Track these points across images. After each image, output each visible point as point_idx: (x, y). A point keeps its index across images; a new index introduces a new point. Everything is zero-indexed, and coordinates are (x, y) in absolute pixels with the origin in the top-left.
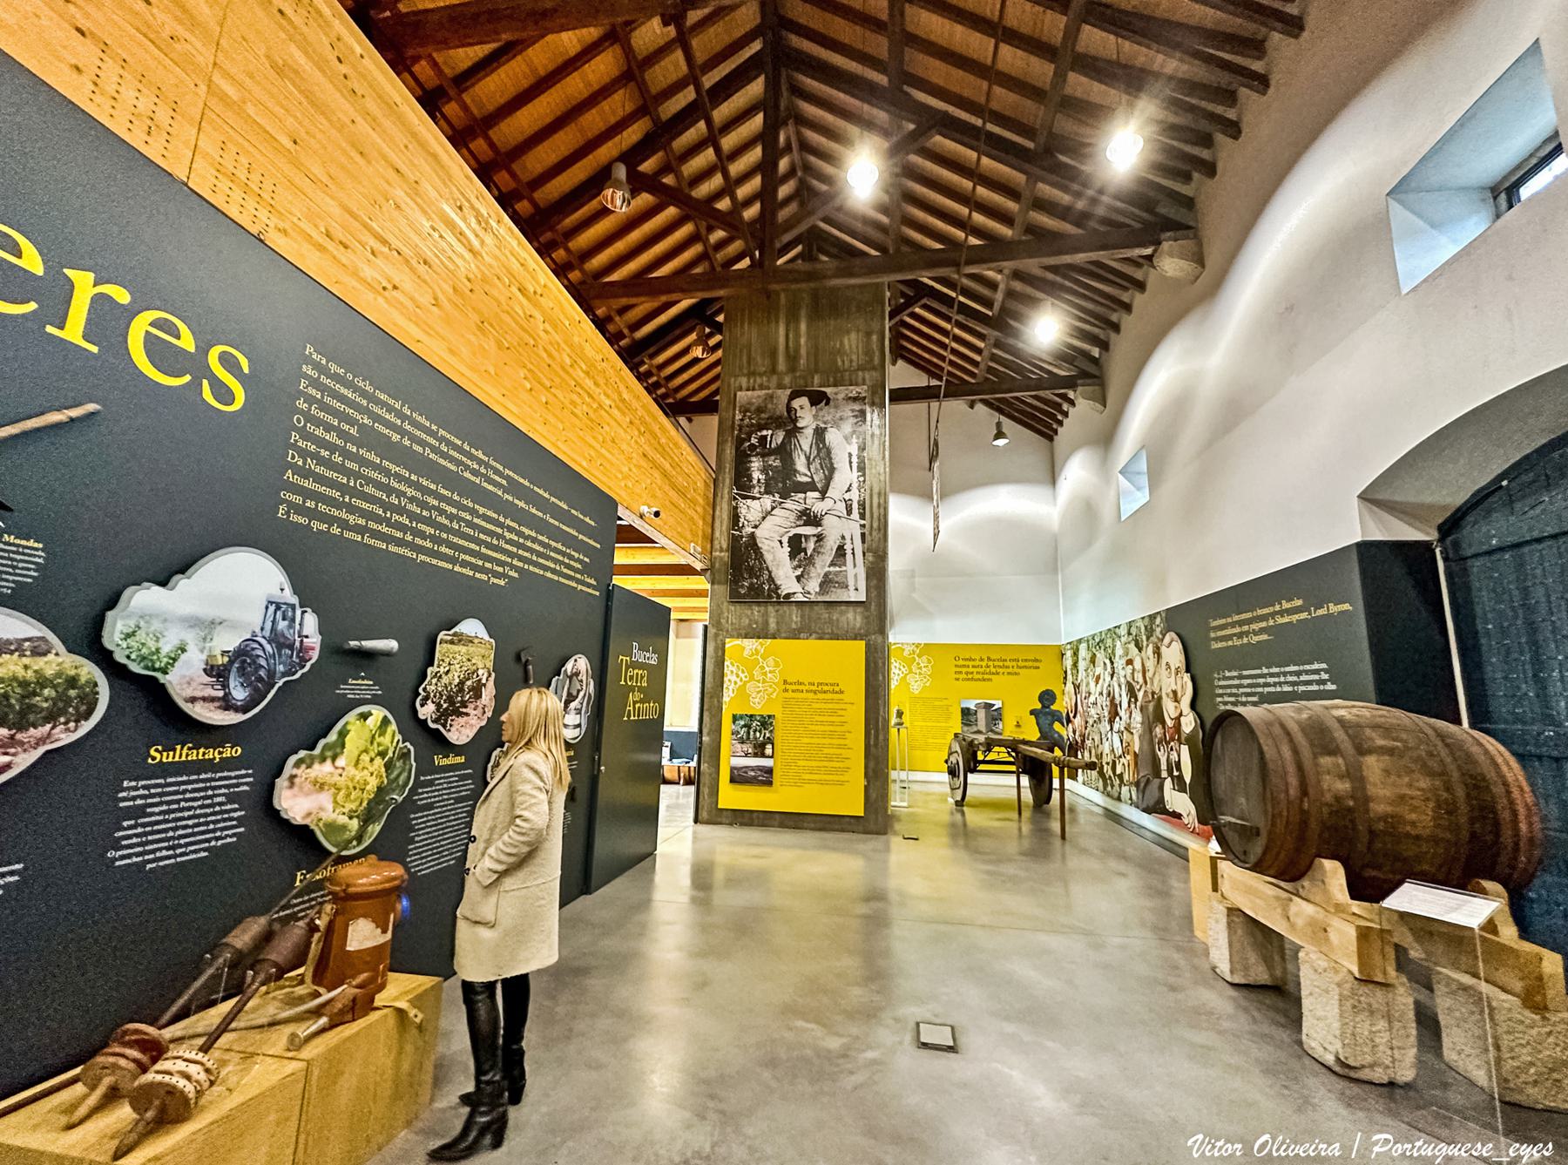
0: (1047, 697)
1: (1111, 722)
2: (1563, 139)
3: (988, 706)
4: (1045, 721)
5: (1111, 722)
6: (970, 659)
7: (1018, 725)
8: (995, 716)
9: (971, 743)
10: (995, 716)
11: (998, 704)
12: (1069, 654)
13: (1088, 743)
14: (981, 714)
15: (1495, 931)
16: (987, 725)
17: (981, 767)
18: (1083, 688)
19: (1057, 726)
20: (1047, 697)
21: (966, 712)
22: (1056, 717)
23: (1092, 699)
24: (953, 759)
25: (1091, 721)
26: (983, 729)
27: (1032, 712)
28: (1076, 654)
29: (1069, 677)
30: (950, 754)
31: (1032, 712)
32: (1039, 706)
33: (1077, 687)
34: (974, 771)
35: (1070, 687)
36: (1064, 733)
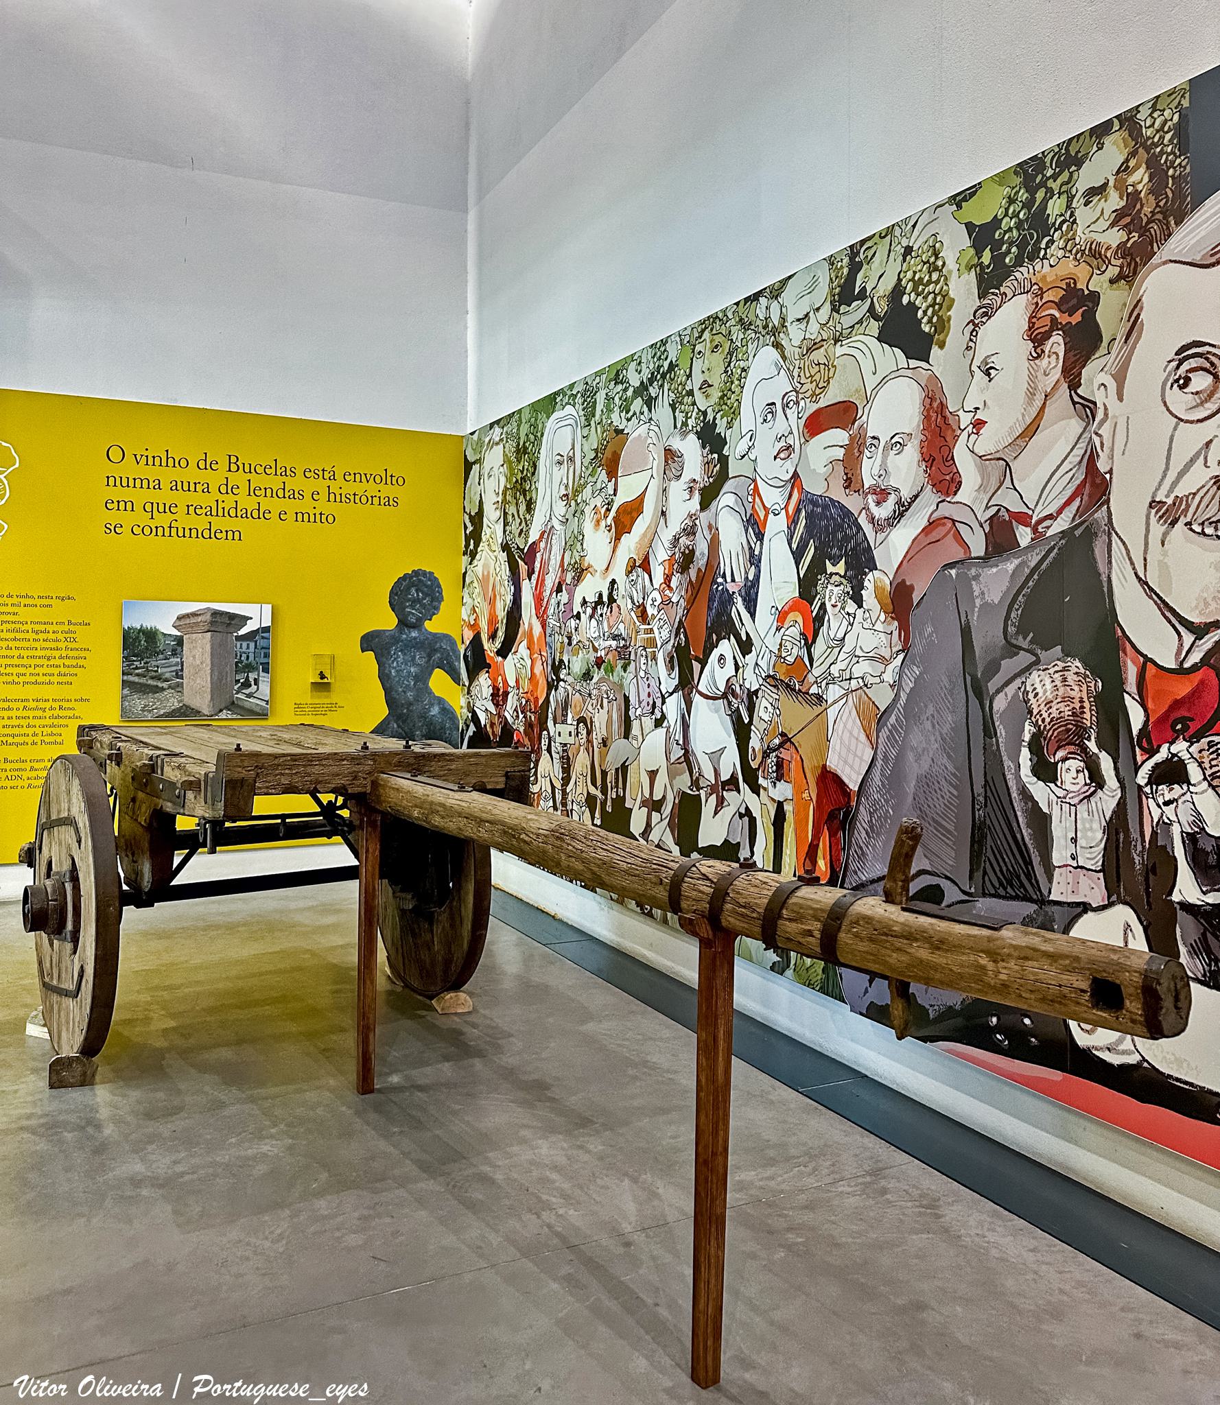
0: (415, 594)
1: (686, 661)
2: (300, 523)
3: (224, 623)
4: (401, 664)
5: (686, 661)
6: (169, 460)
7: (322, 686)
8: (245, 655)
9: (146, 778)
10: (245, 655)
11: (257, 616)
12: (494, 459)
13: (561, 732)
14: (199, 652)
15: (367, 748)
16: (218, 687)
17: (201, 867)
18: (553, 557)
19: (439, 683)
20: (415, 594)
21: (140, 645)
22: (437, 653)
23: (590, 588)
24: (55, 851)
25: (577, 664)
26: (202, 702)
27: (369, 642)
28: (524, 455)
29: (493, 530)
30: (47, 825)
31: (369, 642)
32: (388, 621)
33: (521, 559)
34: (163, 889)
35: (491, 561)
36: (458, 703)
